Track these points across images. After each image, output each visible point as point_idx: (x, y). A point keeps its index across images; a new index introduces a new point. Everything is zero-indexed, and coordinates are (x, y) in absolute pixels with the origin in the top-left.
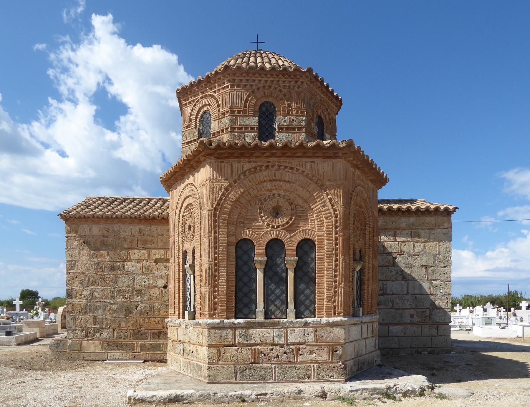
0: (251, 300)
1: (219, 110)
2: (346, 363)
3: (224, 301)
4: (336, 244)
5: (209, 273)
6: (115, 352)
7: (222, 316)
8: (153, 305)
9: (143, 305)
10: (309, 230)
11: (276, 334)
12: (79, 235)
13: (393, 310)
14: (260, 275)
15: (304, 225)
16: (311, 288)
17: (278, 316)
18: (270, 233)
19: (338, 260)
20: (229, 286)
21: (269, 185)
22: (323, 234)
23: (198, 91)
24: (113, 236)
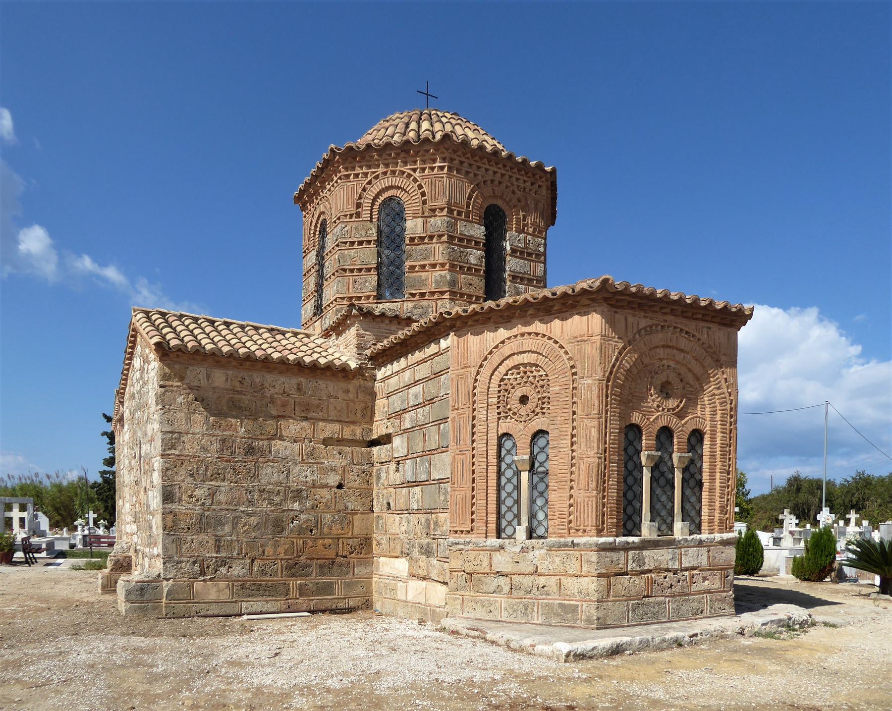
1: (424, 202)
6: (255, 599)
7: (612, 532)
8: (321, 516)
9: (305, 516)
21: (661, 352)
24: (251, 393)
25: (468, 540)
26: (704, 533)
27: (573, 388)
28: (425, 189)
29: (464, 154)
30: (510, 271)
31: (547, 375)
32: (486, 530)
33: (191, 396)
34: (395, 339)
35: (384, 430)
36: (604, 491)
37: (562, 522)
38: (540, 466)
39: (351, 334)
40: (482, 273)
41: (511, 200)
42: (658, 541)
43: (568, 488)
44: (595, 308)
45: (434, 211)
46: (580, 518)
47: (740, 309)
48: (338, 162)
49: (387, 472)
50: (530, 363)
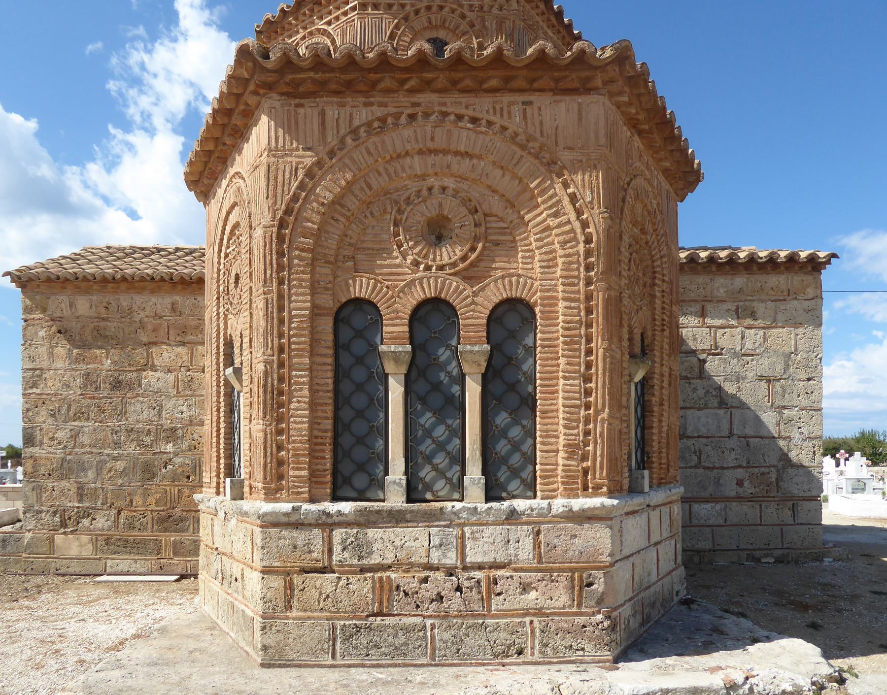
0: (373, 453)
2: (616, 613)
3: (303, 455)
4: (589, 311)
5: (265, 386)
7: (299, 493)
9: (180, 460)
10: (519, 276)
11: (435, 541)
12: (49, 316)
13: (700, 471)
14: (396, 391)
15: (507, 265)
16: (525, 422)
17: (441, 494)
18: (421, 284)
19: (594, 352)
20: (316, 417)
21: (417, 164)
22: (556, 285)
23: (297, 25)
33: (54, 328)
41: (458, 27)
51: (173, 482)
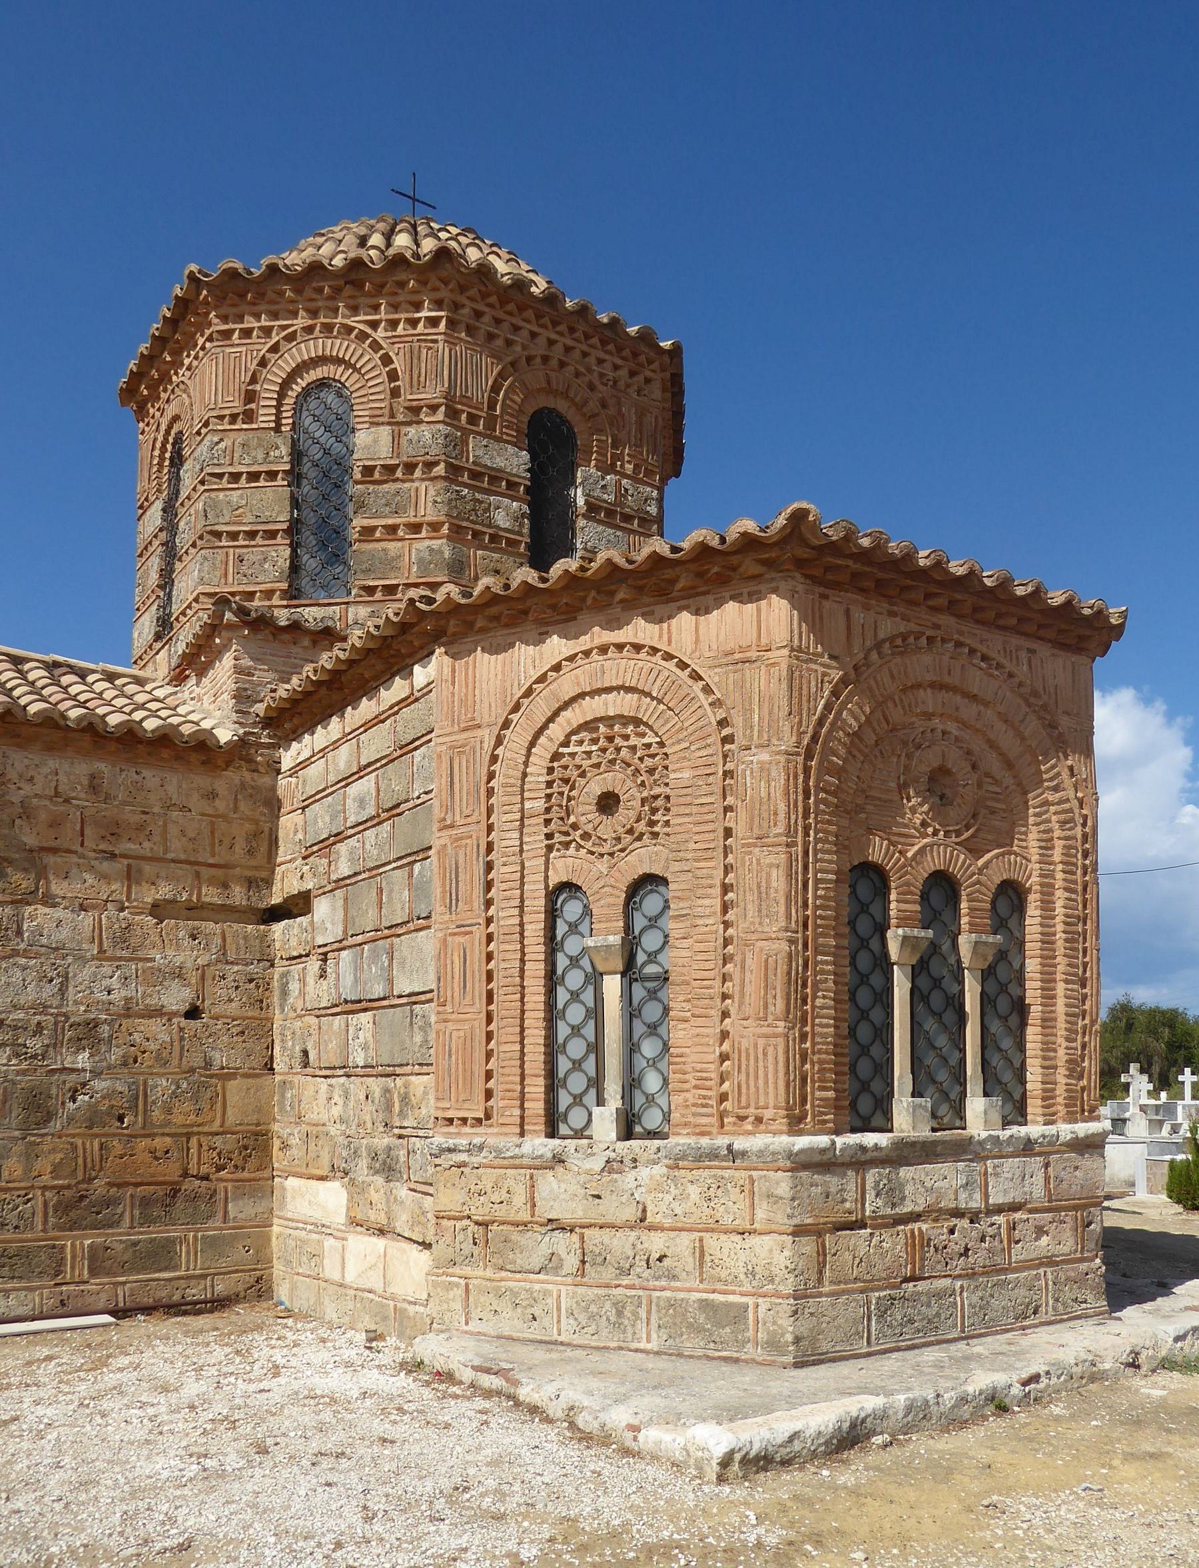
1: (395, 393)
7: (825, 1122)
9: (104, 1084)
21: (928, 699)
25: (477, 1140)
26: (1035, 1122)
27: (725, 773)
28: (399, 364)
29: (484, 296)
30: (585, 549)
31: (661, 744)
32: (522, 1118)
34: (315, 671)
35: (295, 883)
36: (804, 1021)
37: (704, 1097)
38: (649, 962)
39: (224, 670)
40: (522, 548)
41: (585, 403)
42: (934, 1143)
43: (716, 1014)
44: (774, 584)
45: (416, 410)
46: (748, 1088)
47: (1100, 612)
48: (206, 302)
49: (303, 981)
50: (622, 716)
51: (90, 1127)
